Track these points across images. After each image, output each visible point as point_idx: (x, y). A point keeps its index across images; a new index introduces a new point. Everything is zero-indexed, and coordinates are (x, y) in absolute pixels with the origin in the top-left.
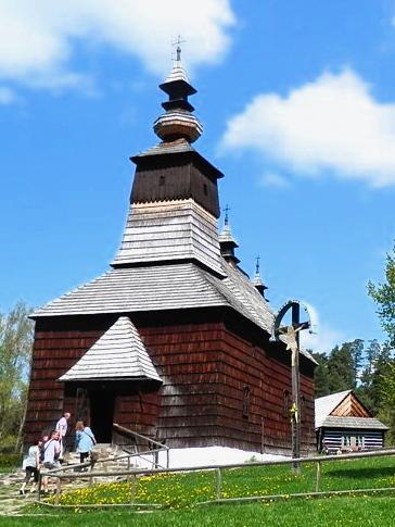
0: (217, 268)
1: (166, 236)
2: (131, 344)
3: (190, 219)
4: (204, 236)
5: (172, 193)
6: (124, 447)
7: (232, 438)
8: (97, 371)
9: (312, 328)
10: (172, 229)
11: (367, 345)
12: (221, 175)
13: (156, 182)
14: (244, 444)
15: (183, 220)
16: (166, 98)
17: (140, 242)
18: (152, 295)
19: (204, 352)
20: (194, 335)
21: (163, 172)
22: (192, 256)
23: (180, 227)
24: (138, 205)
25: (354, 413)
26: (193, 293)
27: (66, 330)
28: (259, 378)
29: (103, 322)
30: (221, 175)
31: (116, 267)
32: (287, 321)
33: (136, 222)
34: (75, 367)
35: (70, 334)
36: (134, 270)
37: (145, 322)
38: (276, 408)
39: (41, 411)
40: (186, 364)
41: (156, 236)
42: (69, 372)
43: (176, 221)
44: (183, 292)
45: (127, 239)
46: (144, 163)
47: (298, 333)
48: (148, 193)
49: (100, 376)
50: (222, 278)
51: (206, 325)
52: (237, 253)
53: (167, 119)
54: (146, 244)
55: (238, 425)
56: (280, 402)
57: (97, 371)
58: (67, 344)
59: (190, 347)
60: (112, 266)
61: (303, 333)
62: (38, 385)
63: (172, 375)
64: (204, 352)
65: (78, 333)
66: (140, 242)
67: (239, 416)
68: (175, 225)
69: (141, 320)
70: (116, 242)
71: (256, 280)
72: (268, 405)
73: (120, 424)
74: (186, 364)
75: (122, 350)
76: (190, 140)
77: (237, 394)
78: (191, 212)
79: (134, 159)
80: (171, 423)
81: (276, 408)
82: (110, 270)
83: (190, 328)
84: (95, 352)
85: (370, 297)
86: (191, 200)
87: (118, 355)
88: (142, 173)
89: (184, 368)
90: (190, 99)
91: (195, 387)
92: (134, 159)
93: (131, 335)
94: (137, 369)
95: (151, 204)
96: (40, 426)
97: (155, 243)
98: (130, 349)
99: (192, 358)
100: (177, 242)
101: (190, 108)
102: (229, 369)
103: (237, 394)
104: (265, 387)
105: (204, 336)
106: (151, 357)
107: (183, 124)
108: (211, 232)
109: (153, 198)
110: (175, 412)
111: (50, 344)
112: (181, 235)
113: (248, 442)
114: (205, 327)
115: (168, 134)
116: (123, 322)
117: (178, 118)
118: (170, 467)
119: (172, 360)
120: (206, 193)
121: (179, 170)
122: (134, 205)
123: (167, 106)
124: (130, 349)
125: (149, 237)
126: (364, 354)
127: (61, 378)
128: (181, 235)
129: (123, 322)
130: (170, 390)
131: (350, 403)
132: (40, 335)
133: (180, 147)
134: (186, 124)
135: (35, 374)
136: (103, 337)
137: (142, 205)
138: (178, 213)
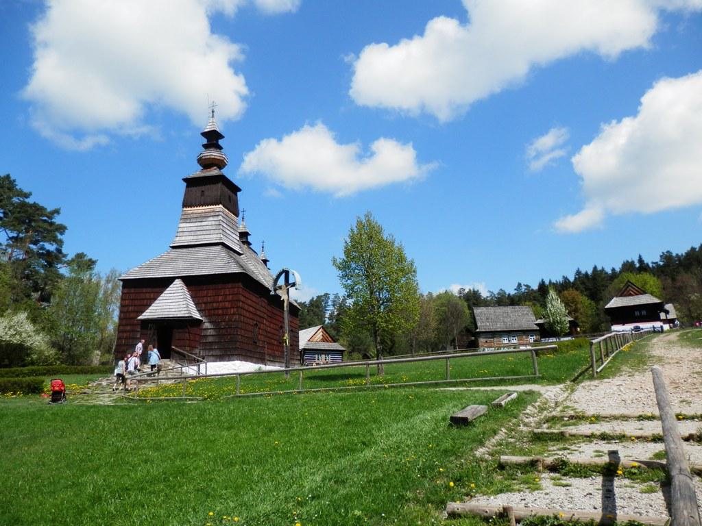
0: (237, 248)
1: (205, 228)
2: (182, 297)
3: (220, 218)
7: (247, 356)
10: (209, 224)
13: (199, 194)
15: (216, 218)
16: (205, 141)
18: (196, 266)
20: (223, 291)
21: (203, 188)
22: (221, 241)
23: (213, 223)
24: (188, 209)
26: (221, 264)
28: (264, 318)
29: (165, 283)
31: (174, 247)
33: (186, 219)
35: (144, 290)
36: (184, 250)
37: (193, 283)
39: (126, 338)
41: (199, 228)
42: (144, 314)
43: (211, 219)
44: (216, 264)
47: (288, 289)
50: (240, 254)
52: (250, 239)
54: (192, 233)
56: (277, 333)
58: (142, 296)
59: (220, 298)
60: (171, 247)
61: (292, 290)
62: (124, 322)
63: (209, 316)
65: (149, 290)
68: (211, 221)
69: (189, 281)
71: (261, 256)
72: (269, 335)
76: (220, 168)
78: (221, 213)
79: (185, 180)
80: (208, 346)
83: (220, 286)
87: (175, 303)
88: (190, 189)
89: (216, 312)
90: (221, 142)
91: (223, 323)
92: (185, 180)
95: (195, 208)
100: (212, 232)
102: (245, 312)
106: (195, 304)
107: (216, 157)
108: (233, 226)
110: (210, 339)
111: (132, 296)
112: (214, 227)
113: (256, 358)
114: (230, 285)
115: (206, 164)
116: (178, 282)
117: (213, 154)
118: (208, 373)
119: (209, 306)
122: (185, 209)
125: (194, 229)
126: (330, 303)
127: (140, 318)
129: (178, 282)
132: (126, 291)
133: (214, 172)
134: (218, 158)
137: (190, 209)
138: (212, 214)
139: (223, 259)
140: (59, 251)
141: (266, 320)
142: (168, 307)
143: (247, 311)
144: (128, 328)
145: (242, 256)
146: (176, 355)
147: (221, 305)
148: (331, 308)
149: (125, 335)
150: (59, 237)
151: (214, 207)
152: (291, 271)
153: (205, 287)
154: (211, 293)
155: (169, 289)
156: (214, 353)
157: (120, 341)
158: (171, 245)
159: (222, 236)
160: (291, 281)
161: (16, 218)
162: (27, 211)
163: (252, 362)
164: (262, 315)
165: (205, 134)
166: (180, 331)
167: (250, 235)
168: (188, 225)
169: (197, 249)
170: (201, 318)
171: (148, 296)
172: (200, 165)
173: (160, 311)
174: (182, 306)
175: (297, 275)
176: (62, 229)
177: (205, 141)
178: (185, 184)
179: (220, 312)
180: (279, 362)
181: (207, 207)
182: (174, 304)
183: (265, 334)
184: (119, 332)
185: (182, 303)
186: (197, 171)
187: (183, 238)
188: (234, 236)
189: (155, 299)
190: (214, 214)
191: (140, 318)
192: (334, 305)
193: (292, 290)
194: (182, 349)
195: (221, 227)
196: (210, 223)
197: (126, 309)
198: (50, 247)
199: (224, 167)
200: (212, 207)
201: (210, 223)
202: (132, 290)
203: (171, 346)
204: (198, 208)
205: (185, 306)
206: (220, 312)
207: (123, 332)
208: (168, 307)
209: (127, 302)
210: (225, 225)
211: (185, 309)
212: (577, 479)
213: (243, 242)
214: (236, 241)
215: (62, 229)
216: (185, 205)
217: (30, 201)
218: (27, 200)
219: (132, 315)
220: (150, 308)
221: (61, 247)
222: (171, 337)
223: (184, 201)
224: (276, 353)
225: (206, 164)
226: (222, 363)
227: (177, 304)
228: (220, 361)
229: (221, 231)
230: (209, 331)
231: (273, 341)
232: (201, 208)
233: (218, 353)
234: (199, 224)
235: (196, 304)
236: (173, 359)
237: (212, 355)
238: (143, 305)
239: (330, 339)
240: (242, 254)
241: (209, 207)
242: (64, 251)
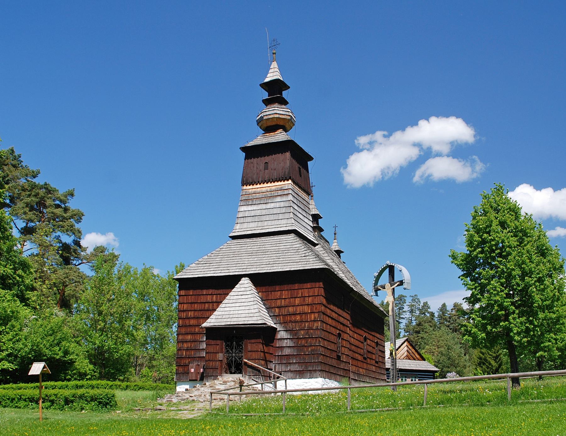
0: (311, 237)
1: (272, 211)
2: (252, 299)
3: (290, 197)
4: (300, 211)
5: (275, 175)
6: (252, 377)
7: (329, 372)
9: (405, 286)
10: (273, 206)
11: (408, 300)
12: (311, 158)
13: (262, 166)
15: (284, 199)
17: (250, 217)
18: (265, 261)
19: (308, 305)
20: (300, 291)
21: (267, 159)
22: (293, 228)
23: (282, 204)
24: (248, 187)
25: (408, 357)
26: (297, 258)
27: (202, 288)
28: (347, 326)
29: (228, 283)
30: (311, 158)
31: (234, 238)
33: (248, 200)
35: (205, 292)
36: (248, 240)
37: (263, 281)
38: (359, 350)
39: (187, 350)
40: (295, 314)
41: (264, 212)
42: (209, 320)
43: (279, 199)
44: (290, 257)
45: (240, 215)
46: (251, 152)
47: (394, 289)
48: (255, 177)
50: (315, 245)
51: (191, 291)
53: (268, 113)
54: (256, 219)
55: (334, 362)
56: (361, 345)
57: (229, 320)
58: (203, 299)
59: (297, 301)
60: (230, 237)
62: (183, 330)
64: (308, 305)
65: (210, 291)
66: (250, 217)
67: (334, 355)
68: (278, 203)
69: (258, 280)
70: (234, 219)
71: (335, 246)
72: (353, 347)
73: (248, 360)
74: (295, 314)
75: (245, 304)
77: (332, 338)
78: (291, 192)
79: (244, 149)
80: (285, 359)
81: (359, 350)
83: (296, 286)
84: (227, 305)
86: (290, 182)
87: (242, 307)
88: (249, 160)
89: (293, 318)
91: (302, 332)
92: (244, 149)
93: (252, 292)
94: (259, 318)
95: (258, 186)
96: (187, 362)
97: (264, 218)
98: (252, 303)
99: (299, 309)
100: (281, 216)
101: (283, 102)
103: (332, 338)
104: (351, 333)
105: (309, 292)
106: (267, 308)
107: (281, 116)
108: (305, 207)
109: (260, 180)
110: (287, 352)
111: (191, 299)
112: (284, 210)
114: (309, 285)
115: (270, 127)
116: (245, 281)
117: (276, 111)
118: (288, 388)
119: (284, 311)
120: (301, 176)
121: (280, 156)
122: (245, 187)
123: (267, 102)
124: (252, 303)
125: (258, 213)
126: (406, 308)
127: (204, 325)
128: (284, 210)
129: (245, 281)
131: (406, 348)
132: (183, 292)
133: (280, 136)
134: (283, 117)
136: (231, 294)
137: (251, 187)
138: (280, 193)
139: (297, 250)
140: (77, 243)
141: (350, 329)
142: (237, 312)
143: (329, 317)
144: (189, 337)
146: (249, 369)
147: (298, 309)
148: (407, 315)
149: (185, 345)
150: (77, 226)
151: (282, 183)
152: (398, 267)
153: (277, 288)
154: (285, 294)
155: (234, 290)
156: (293, 368)
158: (231, 235)
159: (293, 221)
161: (27, 205)
162: (471, 280)
164: (345, 322)
166: (253, 341)
168: (250, 208)
169: (263, 239)
170: (275, 326)
171: (209, 298)
173: (227, 316)
174: (253, 311)
175: (405, 271)
176: (79, 217)
179: (298, 318)
181: (273, 184)
182: (243, 308)
183: (348, 346)
185: (252, 307)
187: (245, 225)
188: (306, 220)
189: (219, 303)
190: (282, 193)
191: (204, 325)
192: (412, 311)
195: (292, 210)
196: (278, 205)
197: (184, 315)
198: (68, 239)
200: (279, 183)
201: (278, 205)
202: (191, 292)
204: (262, 185)
205: (257, 310)
206: (298, 318)
207: (183, 342)
208: (237, 312)
209: (185, 307)
210: (296, 207)
215: (79, 217)
216: (245, 182)
217: (38, 181)
218: (36, 181)
219: (192, 322)
220: (215, 313)
221: (80, 239)
222: (238, 348)
223: (243, 177)
224: (361, 370)
226: (303, 380)
227: (248, 308)
228: (300, 378)
229: (292, 215)
230: (286, 341)
231: (357, 355)
232: (265, 185)
233: (296, 367)
234: (264, 206)
236: (245, 374)
239: (418, 356)
240: (317, 244)
241: (276, 184)
242: (83, 243)
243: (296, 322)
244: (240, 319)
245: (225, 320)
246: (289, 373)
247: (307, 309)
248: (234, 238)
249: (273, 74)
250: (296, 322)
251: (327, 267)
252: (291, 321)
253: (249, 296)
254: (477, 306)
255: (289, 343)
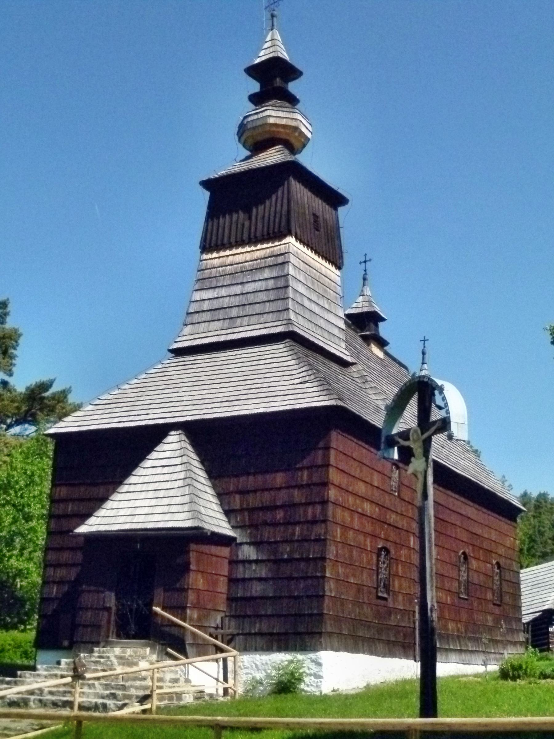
0: (339, 349)
4: (314, 297)
8: (129, 519)
14: (380, 646)
16: (255, 87)
18: (226, 392)
29: (145, 440)
31: (179, 352)
32: (409, 418)
34: (101, 512)
37: (221, 445)
42: (92, 520)
49: (134, 526)
52: (384, 330)
61: (438, 440)
63: (251, 526)
73: (163, 609)
76: (292, 149)
79: (207, 184)
82: (170, 360)
85: (242, 118)
87: (161, 496)
89: (268, 517)
90: (293, 87)
92: (207, 184)
93: (185, 459)
99: (282, 497)
102: (347, 514)
106: (219, 495)
113: (388, 642)
115: (258, 140)
117: (274, 114)
119: (253, 501)
123: (257, 99)
127: (82, 529)
130: (249, 552)
133: (273, 156)
135: (53, 525)
145: (353, 368)
157: (46, 590)
158: (171, 348)
160: (436, 415)
163: (371, 653)
165: (254, 71)
167: (383, 320)
172: (244, 146)
177: (255, 87)
178: (207, 194)
179: (280, 515)
180: (461, 651)
184: (46, 566)
186: (232, 159)
191: (82, 529)
193: (438, 440)
194: (169, 620)
199: (304, 146)
203: (150, 604)
207: (57, 565)
211: (186, 508)
212: (237, 129)
213: (366, 339)
214: (336, 332)
216: (208, 246)
225: (258, 140)
235: (222, 496)
237: (261, 634)
238: (90, 500)
243: (275, 524)
244: (136, 519)
245: (122, 520)
246: (258, 639)
247: (297, 496)
248: (179, 352)
249: (273, 46)
250: (275, 524)
251: (340, 403)
252: (265, 523)
253: (178, 468)
254: (33, 595)
255: (263, 571)
